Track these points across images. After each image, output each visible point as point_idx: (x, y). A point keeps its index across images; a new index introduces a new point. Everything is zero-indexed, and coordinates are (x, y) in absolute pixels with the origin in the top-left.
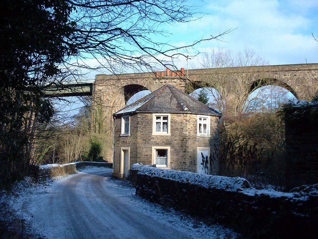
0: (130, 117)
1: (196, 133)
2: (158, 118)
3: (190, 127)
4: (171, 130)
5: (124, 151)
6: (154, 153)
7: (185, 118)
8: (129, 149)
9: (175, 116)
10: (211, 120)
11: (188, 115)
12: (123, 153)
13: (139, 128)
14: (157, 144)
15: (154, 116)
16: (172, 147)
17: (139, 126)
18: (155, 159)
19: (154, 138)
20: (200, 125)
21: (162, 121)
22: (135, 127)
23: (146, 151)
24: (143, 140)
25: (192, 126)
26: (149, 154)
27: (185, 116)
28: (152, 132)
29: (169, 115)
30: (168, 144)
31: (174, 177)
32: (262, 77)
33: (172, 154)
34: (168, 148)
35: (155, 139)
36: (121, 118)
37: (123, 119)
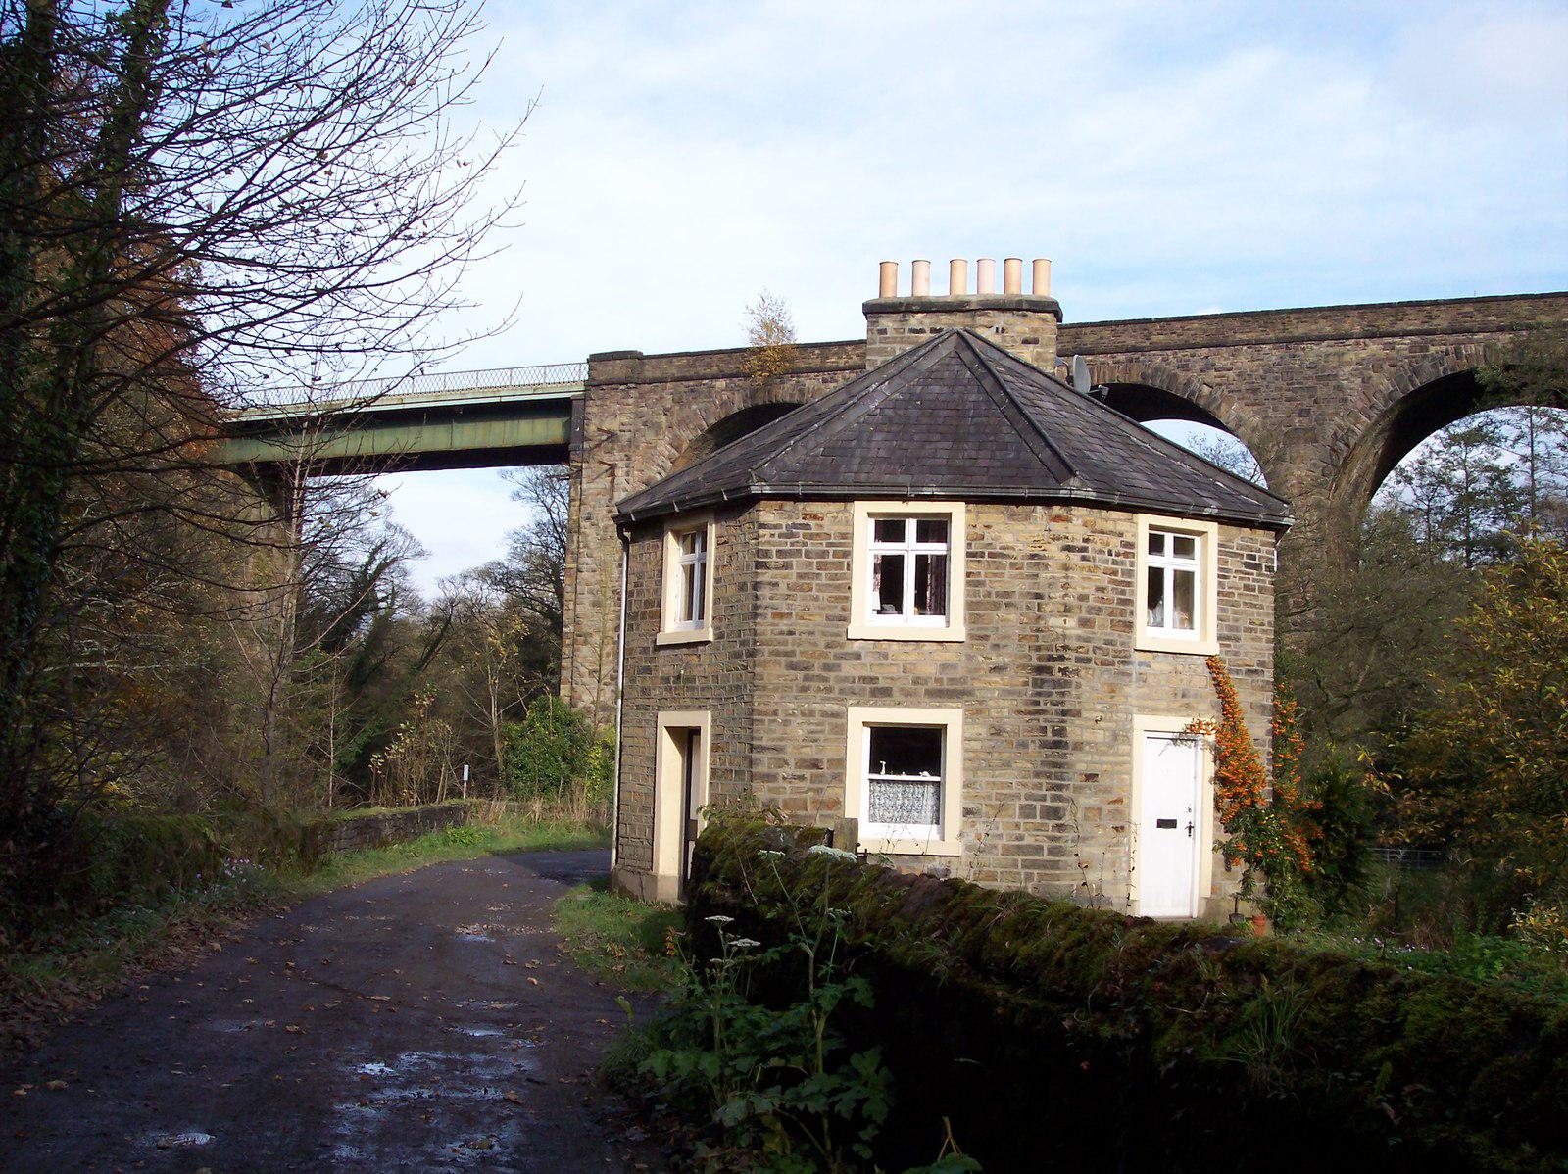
0: (713, 531)
1: (1129, 626)
2: (889, 529)
3: (1090, 591)
4: (970, 605)
5: (686, 738)
6: (859, 748)
7: (1058, 528)
8: (704, 720)
9: (993, 515)
10: (1223, 547)
11: (1079, 512)
12: (670, 756)
13: (765, 592)
14: (881, 694)
15: (862, 516)
16: (973, 714)
17: (766, 576)
18: (712, 580)
19: (858, 656)
20: (1156, 576)
21: (910, 548)
22: (742, 587)
23: (812, 738)
24: (792, 667)
25: (1104, 580)
26: (829, 752)
27: (1058, 519)
28: (845, 620)
29: (958, 511)
30: (941, 694)
31: (890, 934)
32: (1474, 352)
33: (973, 763)
34: (950, 717)
35: (866, 659)
36: (661, 537)
37: (670, 539)
